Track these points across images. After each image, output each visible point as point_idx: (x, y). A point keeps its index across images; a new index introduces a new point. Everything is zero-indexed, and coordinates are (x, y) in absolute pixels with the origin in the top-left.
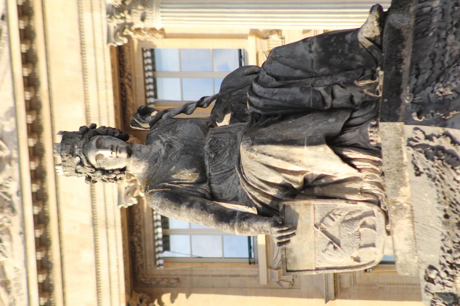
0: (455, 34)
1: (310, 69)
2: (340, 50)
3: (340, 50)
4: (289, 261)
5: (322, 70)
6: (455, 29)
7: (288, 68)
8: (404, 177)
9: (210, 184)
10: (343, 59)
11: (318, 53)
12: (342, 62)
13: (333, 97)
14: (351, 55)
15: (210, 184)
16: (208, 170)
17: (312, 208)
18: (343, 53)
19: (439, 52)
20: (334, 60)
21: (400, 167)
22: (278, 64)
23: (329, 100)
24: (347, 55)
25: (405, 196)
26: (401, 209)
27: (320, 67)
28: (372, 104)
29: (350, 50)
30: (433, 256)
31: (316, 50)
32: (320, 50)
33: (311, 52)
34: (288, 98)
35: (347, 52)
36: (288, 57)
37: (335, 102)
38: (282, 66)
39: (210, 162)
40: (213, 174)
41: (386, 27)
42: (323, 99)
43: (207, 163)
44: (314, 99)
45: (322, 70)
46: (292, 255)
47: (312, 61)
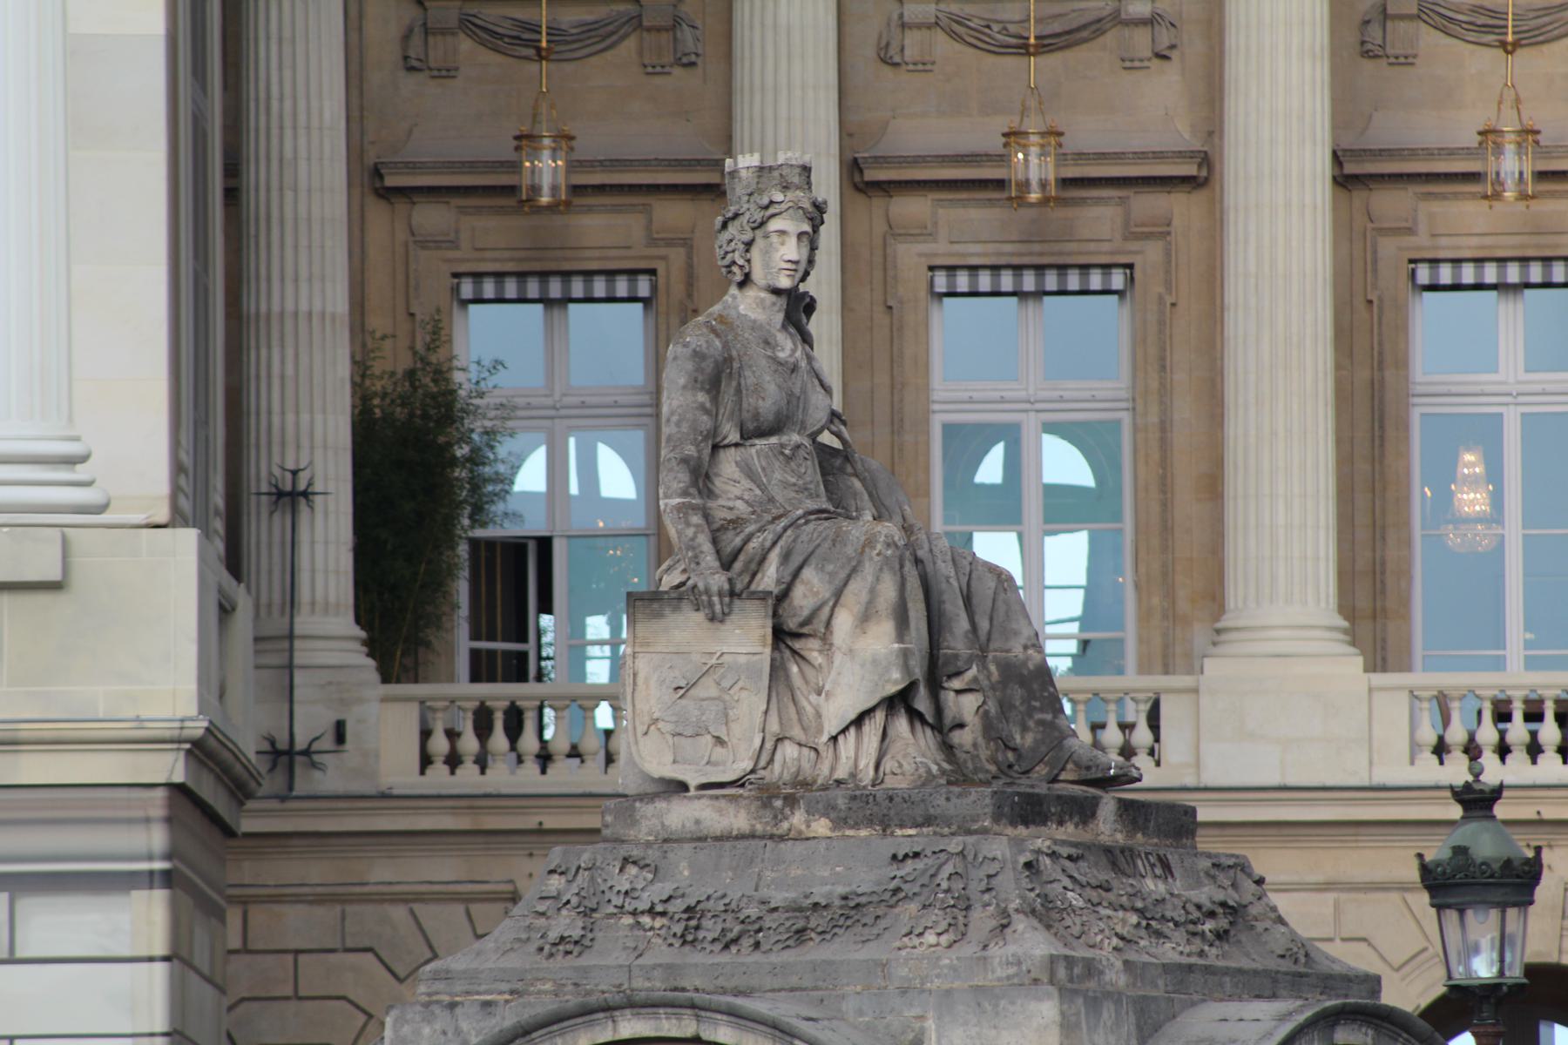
0: (1138, 925)
1: (992, 646)
2: (1037, 704)
3: (1037, 704)
4: (656, 606)
5: (993, 668)
6: (1144, 923)
7: (989, 603)
8: (856, 826)
9: (736, 445)
10: (1022, 709)
11: (1024, 663)
12: (1015, 707)
13: (958, 692)
14: (1031, 724)
15: (736, 445)
16: (760, 443)
17: (759, 649)
18: (1030, 711)
19: (1111, 896)
20: (1017, 694)
21: (881, 822)
22: (992, 584)
23: (957, 684)
24: (1031, 717)
25: (808, 826)
26: (775, 817)
27: (998, 665)
28: (949, 762)
29: (1041, 723)
30: (686, 873)
31: (1028, 658)
32: (1031, 666)
33: (1026, 648)
34: (948, 607)
35: (1039, 716)
36: (1006, 603)
37: (952, 694)
38: (990, 592)
39: (771, 448)
40: (753, 450)
41: (1092, 791)
42: (958, 674)
43: (774, 440)
44: (956, 657)
45: (993, 668)
46: (667, 611)
47: (1008, 651)
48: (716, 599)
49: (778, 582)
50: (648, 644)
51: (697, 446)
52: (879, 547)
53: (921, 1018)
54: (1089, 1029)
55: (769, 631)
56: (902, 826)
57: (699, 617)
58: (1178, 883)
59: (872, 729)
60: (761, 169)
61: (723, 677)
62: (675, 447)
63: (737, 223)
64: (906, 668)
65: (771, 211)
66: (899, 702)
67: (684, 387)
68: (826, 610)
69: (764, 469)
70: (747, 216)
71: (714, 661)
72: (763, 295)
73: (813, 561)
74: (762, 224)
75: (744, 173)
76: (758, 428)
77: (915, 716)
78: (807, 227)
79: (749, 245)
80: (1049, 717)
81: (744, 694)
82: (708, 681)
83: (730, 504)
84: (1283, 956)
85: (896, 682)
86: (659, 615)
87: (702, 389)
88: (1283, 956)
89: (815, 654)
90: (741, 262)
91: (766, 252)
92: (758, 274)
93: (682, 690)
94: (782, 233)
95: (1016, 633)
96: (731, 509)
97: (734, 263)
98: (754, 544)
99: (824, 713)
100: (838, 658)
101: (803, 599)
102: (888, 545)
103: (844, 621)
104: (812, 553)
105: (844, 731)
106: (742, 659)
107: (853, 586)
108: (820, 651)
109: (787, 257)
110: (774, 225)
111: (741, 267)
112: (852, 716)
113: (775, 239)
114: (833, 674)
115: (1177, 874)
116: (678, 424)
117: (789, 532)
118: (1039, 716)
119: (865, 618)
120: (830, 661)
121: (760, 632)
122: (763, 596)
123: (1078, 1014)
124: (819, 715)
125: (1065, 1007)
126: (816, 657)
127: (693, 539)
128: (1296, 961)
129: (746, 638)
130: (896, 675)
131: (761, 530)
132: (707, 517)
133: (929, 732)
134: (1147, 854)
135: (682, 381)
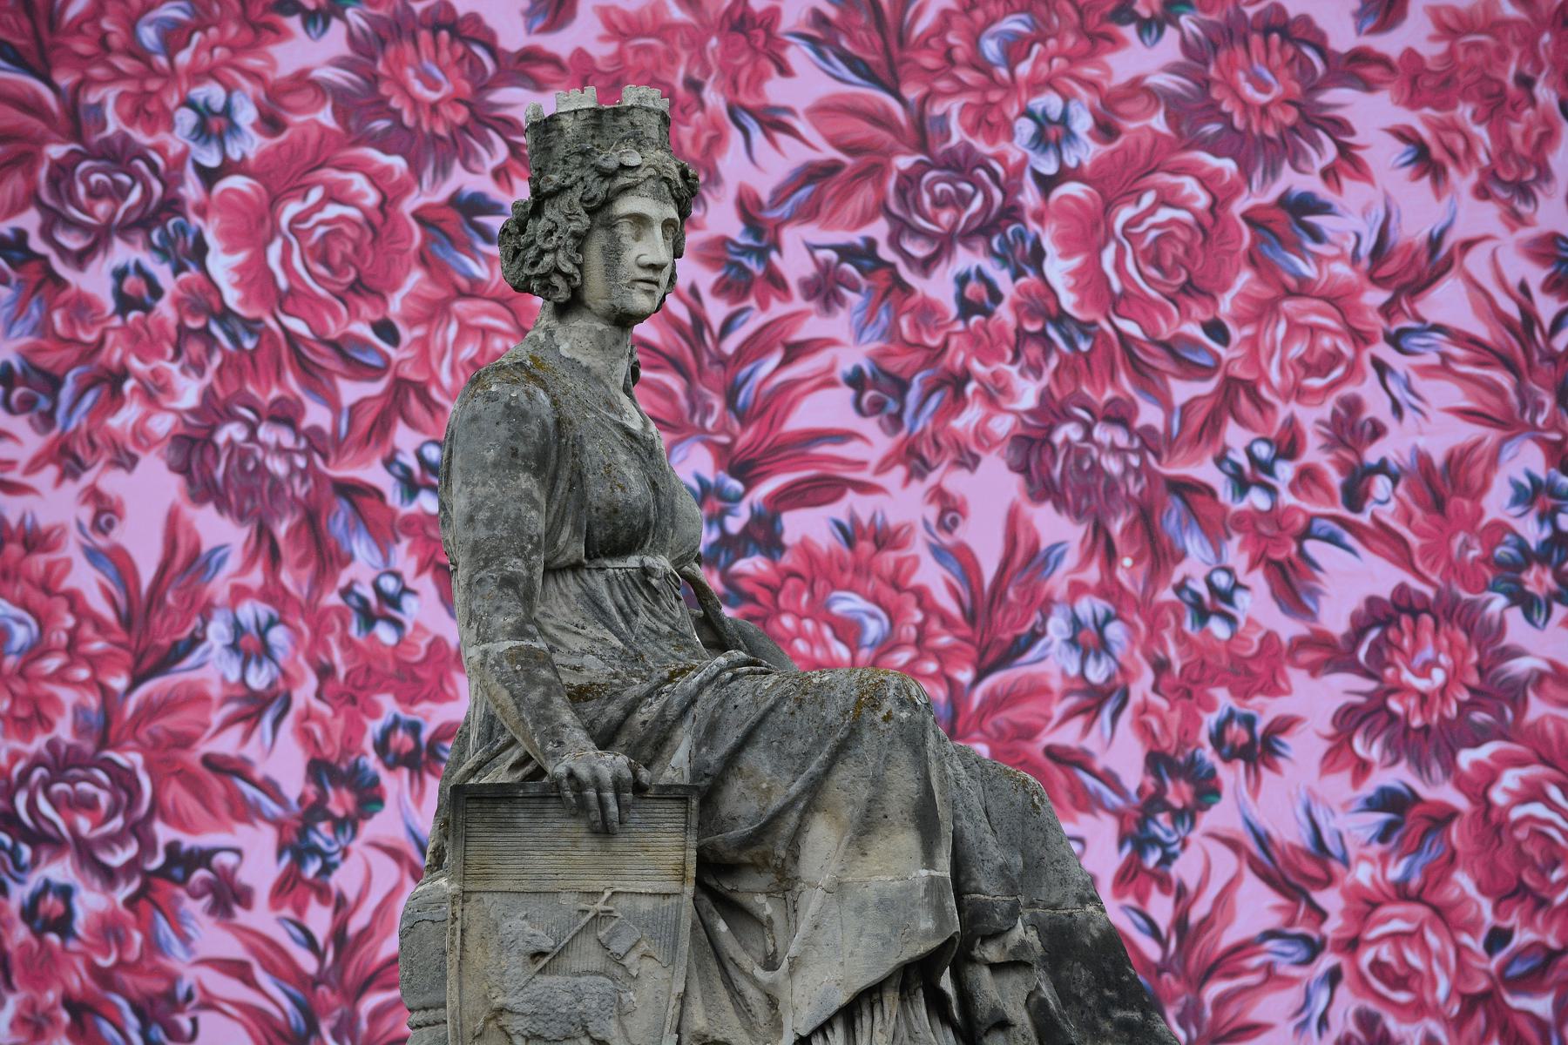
4: (503, 809)
13: (995, 968)
17: (674, 886)
23: (992, 952)
24: (1107, 1016)
35: (1119, 1014)
37: (986, 971)
46: (522, 818)
48: (609, 795)
49: (696, 773)
50: (487, 877)
51: (527, 559)
52: (887, 705)
55: (692, 854)
57: (577, 828)
60: (597, 113)
61: (614, 935)
62: (487, 563)
63: (563, 202)
64: (939, 911)
65: (622, 181)
66: (915, 977)
67: (495, 465)
68: (792, 819)
69: (620, 609)
70: (579, 190)
71: (600, 906)
72: (600, 326)
73: (762, 737)
74: (608, 202)
75: (567, 123)
76: (613, 537)
77: (937, 1004)
78: (672, 212)
79: (581, 239)
80: (1137, 1016)
81: (648, 964)
82: (588, 944)
83: (575, 661)
85: (926, 935)
86: (507, 825)
87: (527, 468)
89: (760, 899)
90: (568, 268)
91: (613, 254)
92: (596, 288)
94: (640, 220)
96: (577, 669)
97: (557, 271)
98: (646, 713)
99: (784, 997)
100: (812, 903)
101: (740, 806)
102: (903, 703)
103: (823, 843)
104: (762, 720)
105: (823, 1028)
106: (645, 905)
107: (844, 774)
108: (769, 894)
109: (646, 260)
110: (627, 205)
111: (567, 277)
112: (841, 998)
113: (625, 230)
114: (804, 927)
116: (490, 524)
117: (708, 692)
118: (1119, 1014)
119: (866, 827)
120: (792, 910)
121: (674, 856)
122: (669, 793)
124: (773, 1003)
126: (766, 907)
127: (542, 706)
129: (657, 863)
130: (926, 923)
131: (655, 691)
132: (1489, 64)
133: (949, 1032)
135: (491, 455)
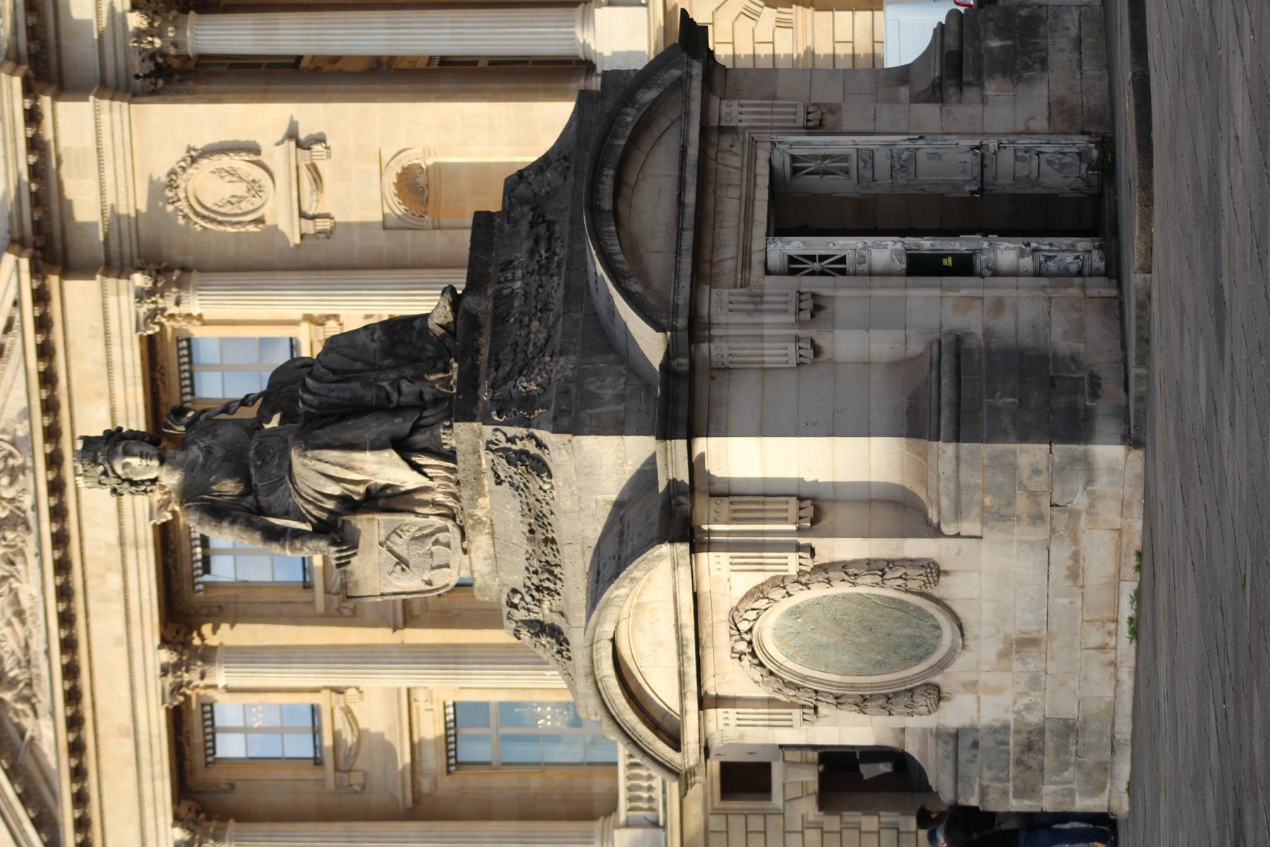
0: (539, 320)
4: (350, 585)
5: (387, 362)
8: (483, 487)
14: (420, 344)
15: (256, 496)
16: (255, 480)
17: (376, 523)
19: (521, 341)
20: (400, 350)
23: (395, 396)
31: (379, 339)
33: (373, 340)
37: (402, 399)
42: (388, 395)
43: (253, 471)
45: (387, 362)
46: (353, 578)
53: (596, 502)
54: (601, 405)
56: (480, 465)
58: (518, 255)
59: (422, 460)
84: (565, 178)
88: (565, 178)
93: (402, 562)
95: (364, 345)
115: (512, 257)
123: (590, 416)
125: (586, 430)
128: (568, 168)
129: (371, 527)
134: (499, 283)
